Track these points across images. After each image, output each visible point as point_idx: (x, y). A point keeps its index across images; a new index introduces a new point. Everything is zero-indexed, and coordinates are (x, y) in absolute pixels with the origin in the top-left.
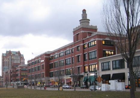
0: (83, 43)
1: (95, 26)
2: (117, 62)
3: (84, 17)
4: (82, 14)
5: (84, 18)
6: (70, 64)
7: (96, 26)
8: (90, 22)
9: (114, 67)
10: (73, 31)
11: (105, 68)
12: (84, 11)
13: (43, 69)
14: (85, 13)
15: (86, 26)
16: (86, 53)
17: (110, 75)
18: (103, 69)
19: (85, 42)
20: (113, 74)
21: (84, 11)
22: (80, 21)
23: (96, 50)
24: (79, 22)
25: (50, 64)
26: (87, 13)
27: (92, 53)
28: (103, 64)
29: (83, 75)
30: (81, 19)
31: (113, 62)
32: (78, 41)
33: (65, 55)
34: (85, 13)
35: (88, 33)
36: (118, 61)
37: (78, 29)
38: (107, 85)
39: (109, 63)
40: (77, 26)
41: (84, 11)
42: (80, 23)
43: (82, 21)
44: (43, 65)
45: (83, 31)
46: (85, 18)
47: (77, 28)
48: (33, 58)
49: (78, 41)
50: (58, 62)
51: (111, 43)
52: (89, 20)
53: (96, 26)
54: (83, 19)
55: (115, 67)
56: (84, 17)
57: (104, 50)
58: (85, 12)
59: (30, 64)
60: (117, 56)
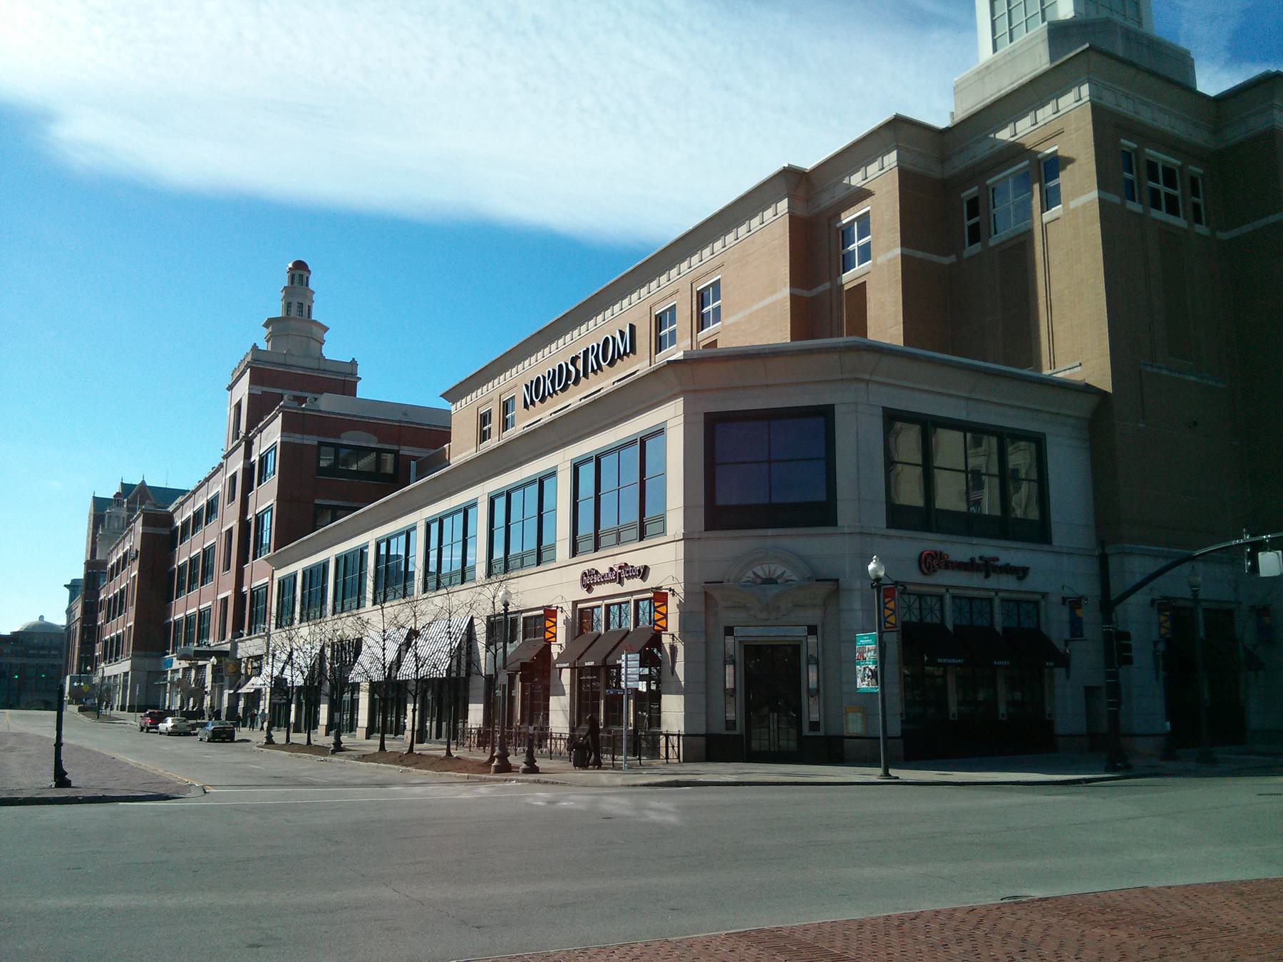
7: (354, 363)
8: (326, 336)
26: (313, 285)
57: (317, 501)
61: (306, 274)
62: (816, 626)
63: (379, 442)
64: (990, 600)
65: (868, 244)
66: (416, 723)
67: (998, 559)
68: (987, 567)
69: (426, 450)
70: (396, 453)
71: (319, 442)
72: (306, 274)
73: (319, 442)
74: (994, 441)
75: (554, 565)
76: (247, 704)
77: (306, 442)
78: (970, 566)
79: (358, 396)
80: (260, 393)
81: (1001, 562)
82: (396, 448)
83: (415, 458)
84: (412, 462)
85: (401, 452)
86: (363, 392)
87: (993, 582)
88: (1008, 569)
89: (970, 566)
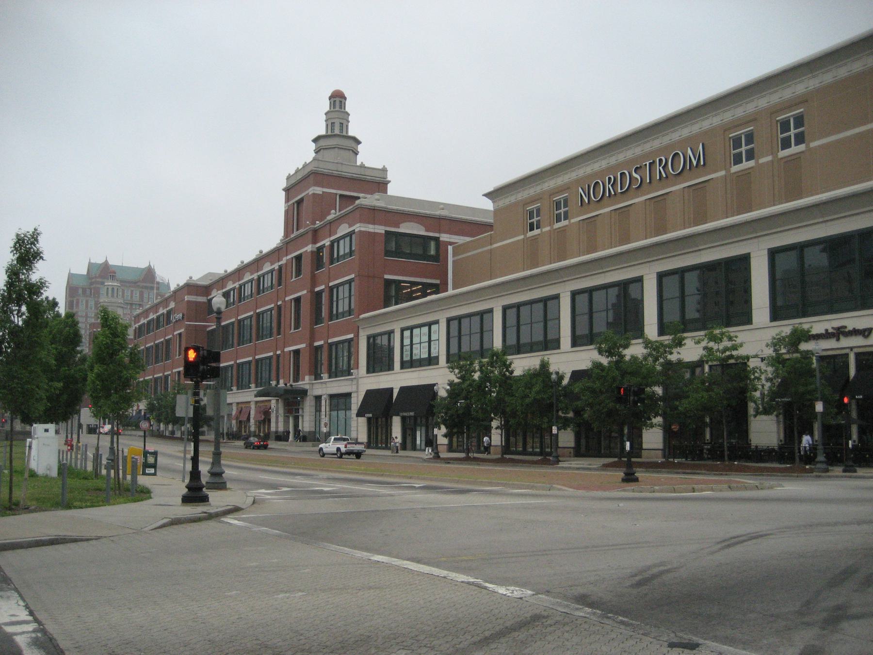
0: (315, 242)
1: (380, 167)
2: (692, 282)
3: (333, 124)
4: (328, 109)
5: (332, 130)
6: (350, 312)
7: (384, 170)
8: (360, 148)
9: (583, 330)
10: (284, 185)
11: (524, 339)
12: (338, 99)
13: (297, 326)
14: (337, 108)
15: (332, 167)
16: (323, 287)
17: (391, 390)
18: (454, 349)
19: (322, 240)
20: (403, 390)
21: (338, 99)
22: (315, 140)
23: (353, 276)
24: (313, 146)
25: (209, 332)
26: (349, 108)
27: (341, 288)
28: (407, 333)
29: (307, 387)
30: (323, 132)
31: (508, 312)
32: (301, 231)
33: (258, 293)
34: (337, 108)
35: (341, 196)
36: (695, 273)
37: (299, 177)
38: (443, 434)
39: (392, 335)
40: (292, 172)
41: (338, 100)
42: (317, 152)
43: (322, 143)
44: (298, 300)
45: (318, 190)
46: (337, 132)
47: (297, 171)
48: (265, 251)
49: (301, 231)
50: (271, 310)
51: (426, 248)
52: (358, 142)
53: (384, 170)
54: (329, 133)
55: (586, 331)
56: (333, 124)
57: (387, 277)
58: (342, 105)
59: (248, 291)
60: (432, 301)
61: (343, 100)
62: (752, 324)
63: (427, 231)
64: (847, 355)
65: (753, 149)
66: (816, 221)
67: (846, 327)
68: (840, 333)
69: (462, 238)
70: (437, 239)
71: (385, 231)
72: (343, 100)
73: (385, 231)
74: (153, 472)
75: (437, 366)
76: (387, 421)
77: (376, 231)
78: (827, 335)
79: (389, 193)
80: (321, 193)
81: (850, 328)
82: (437, 235)
83: (451, 243)
84: (449, 247)
85: (441, 239)
86: (392, 190)
87: (846, 342)
88: (855, 332)
89: (827, 335)
